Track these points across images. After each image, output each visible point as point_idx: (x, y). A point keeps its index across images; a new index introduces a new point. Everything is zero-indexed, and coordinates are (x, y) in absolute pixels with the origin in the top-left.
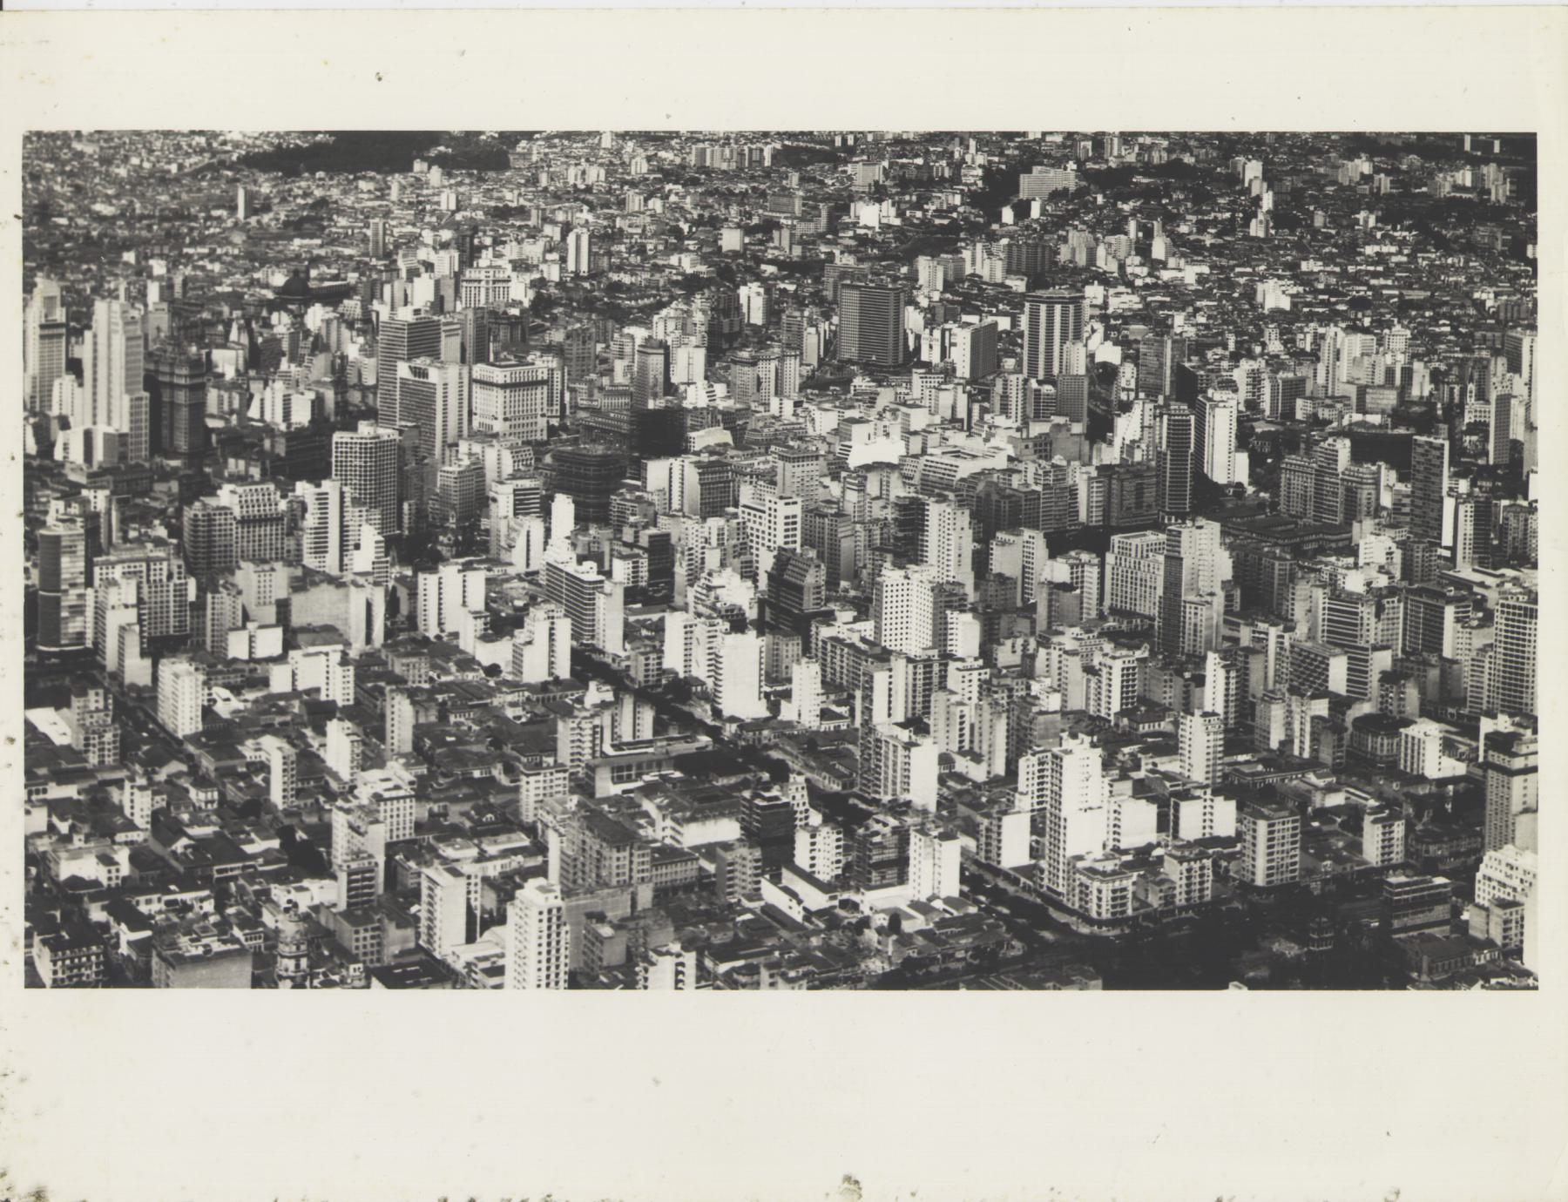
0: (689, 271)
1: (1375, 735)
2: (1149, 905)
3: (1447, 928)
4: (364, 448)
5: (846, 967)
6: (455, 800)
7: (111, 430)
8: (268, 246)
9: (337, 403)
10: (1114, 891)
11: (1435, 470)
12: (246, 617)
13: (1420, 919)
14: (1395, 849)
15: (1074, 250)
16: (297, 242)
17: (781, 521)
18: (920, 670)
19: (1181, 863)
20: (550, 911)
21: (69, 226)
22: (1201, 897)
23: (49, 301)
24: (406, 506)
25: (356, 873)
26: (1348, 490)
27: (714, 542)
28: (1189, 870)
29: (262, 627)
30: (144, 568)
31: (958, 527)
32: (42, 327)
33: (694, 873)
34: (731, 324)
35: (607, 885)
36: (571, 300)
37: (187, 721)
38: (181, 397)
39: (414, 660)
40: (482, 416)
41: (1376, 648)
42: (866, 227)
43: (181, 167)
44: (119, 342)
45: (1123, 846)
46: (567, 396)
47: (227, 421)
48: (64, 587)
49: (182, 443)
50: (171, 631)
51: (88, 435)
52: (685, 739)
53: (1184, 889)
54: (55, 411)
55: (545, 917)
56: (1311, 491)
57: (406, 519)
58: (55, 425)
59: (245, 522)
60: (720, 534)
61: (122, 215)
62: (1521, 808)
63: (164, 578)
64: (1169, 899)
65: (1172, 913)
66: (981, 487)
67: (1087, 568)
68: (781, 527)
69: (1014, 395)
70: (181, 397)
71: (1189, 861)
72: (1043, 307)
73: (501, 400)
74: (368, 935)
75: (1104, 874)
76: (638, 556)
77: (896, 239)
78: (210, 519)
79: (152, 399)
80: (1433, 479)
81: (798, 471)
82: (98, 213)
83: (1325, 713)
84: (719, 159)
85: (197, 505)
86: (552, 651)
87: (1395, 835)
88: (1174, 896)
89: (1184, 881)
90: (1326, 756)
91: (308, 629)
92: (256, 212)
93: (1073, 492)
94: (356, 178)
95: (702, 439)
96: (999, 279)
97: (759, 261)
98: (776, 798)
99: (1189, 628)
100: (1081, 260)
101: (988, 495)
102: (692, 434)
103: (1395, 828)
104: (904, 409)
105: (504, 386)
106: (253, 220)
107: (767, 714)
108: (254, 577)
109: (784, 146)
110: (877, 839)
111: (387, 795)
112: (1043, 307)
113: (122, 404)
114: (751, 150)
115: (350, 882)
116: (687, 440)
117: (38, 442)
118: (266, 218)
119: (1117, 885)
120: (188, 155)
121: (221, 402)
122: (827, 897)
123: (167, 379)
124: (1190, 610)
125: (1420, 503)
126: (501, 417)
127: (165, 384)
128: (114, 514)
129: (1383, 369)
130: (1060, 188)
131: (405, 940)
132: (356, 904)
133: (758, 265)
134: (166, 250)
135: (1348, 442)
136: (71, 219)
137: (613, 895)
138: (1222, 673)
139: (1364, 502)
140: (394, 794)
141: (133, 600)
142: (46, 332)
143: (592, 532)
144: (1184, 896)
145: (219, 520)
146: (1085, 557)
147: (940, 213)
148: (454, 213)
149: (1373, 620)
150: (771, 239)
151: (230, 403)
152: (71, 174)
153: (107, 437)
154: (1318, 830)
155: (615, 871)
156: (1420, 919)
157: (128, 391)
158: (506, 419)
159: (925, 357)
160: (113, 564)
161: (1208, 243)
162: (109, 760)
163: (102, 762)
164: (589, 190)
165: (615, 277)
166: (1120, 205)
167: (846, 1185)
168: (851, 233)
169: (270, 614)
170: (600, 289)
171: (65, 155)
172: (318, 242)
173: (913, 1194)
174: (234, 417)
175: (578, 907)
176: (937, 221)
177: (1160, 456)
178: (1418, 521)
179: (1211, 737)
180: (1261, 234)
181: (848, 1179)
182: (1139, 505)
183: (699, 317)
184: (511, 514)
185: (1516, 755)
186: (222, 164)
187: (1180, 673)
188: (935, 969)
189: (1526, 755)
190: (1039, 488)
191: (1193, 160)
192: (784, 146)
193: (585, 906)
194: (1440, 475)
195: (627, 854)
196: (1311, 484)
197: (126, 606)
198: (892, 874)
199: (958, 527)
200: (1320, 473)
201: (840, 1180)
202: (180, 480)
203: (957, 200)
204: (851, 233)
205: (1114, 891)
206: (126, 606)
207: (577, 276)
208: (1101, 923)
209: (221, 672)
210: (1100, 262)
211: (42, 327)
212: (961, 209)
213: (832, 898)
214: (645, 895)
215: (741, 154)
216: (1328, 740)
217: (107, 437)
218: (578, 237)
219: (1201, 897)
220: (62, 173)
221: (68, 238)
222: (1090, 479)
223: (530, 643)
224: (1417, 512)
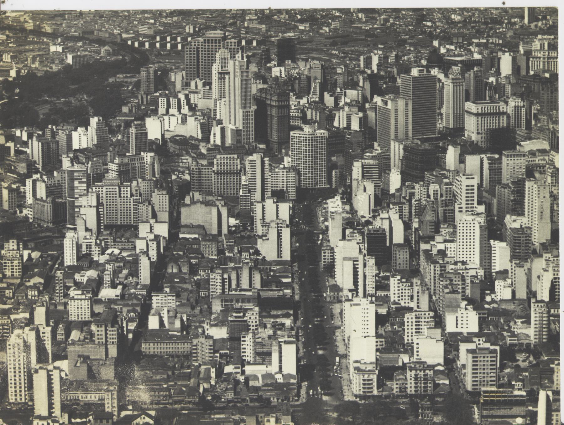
7: (234, 128)
10: (364, 380)
12: (154, 216)
13: (502, 412)
17: (464, 188)
22: (426, 391)
24: (334, 173)
28: (416, 375)
30: (117, 189)
31: (542, 197)
32: (219, 73)
35: (92, 342)
37: (69, 261)
48: (76, 196)
63: (129, 196)
70: (274, 112)
75: (364, 371)
81: (511, 162)
88: (406, 388)
91: (186, 226)
105: (477, 115)
106: (533, 25)
118: (540, 24)
126: (475, 132)
128: (156, 165)
134: (460, 40)
137: (94, 348)
141: (94, 203)
144: (413, 389)
156: (502, 412)
157: (242, 108)
158: (478, 133)
160: (102, 186)
162: (16, 274)
163: (12, 275)
184: (360, 178)
193: (79, 351)
195: (103, 329)
197: (91, 207)
202: (264, 157)
206: (91, 207)
213: (236, 368)
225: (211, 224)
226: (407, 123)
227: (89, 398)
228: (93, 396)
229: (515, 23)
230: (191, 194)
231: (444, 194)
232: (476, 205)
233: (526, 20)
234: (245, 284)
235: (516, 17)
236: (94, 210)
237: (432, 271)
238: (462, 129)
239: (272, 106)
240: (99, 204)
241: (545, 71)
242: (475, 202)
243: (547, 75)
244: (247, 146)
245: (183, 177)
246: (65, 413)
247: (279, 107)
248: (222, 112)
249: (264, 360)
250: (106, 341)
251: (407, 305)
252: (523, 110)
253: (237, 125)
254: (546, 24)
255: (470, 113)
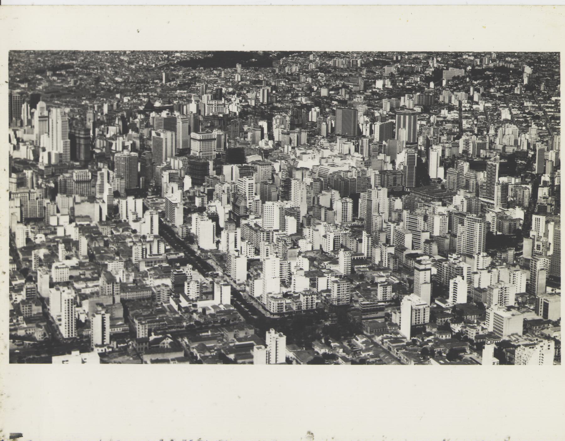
0: (304, 103)
1: (411, 260)
2: (292, 309)
3: (383, 319)
4: (125, 158)
5: (177, 323)
6: (88, 270)
7: (57, 152)
8: (168, 93)
9: (140, 145)
10: (278, 304)
11: (493, 174)
12: (58, 211)
14: (388, 295)
15: (444, 97)
16: (178, 91)
17: (247, 185)
18: (265, 234)
19: (304, 296)
20: (68, 300)
21: (105, 85)
22: (312, 307)
23: (42, 108)
24: (141, 179)
25: (29, 289)
26: (467, 180)
27: (226, 192)
28: (307, 299)
29: (62, 215)
31: (301, 189)
32: (39, 117)
33: (150, 294)
34: (298, 121)
36: (256, 112)
38: (82, 141)
39: (106, 227)
40: (194, 150)
41: (423, 231)
42: (378, 89)
43: (156, 65)
44: (60, 122)
45: (296, 291)
46: (227, 144)
47: (102, 150)
49: (82, 157)
50: (38, 216)
51: (49, 154)
52: (176, 254)
53: (305, 304)
54: (42, 146)
55: (67, 302)
56: (456, 181)
57: (141, 183)
58: (41, 150)
59: (78, 182)
60: (228, 189)
61: (124, 82)
62: (424, 282)
64: (299, 307)
65: (301, 312)
66: (335, 176)
67: (348, 204)
68: (247, 187)
69: (365, 146)
70: (82, 141)
71: (307, 295)
72: (402, 116)
73: (199, 145)
74: (27, 308)
75: (277, 298)
76: (204, 196)
77: (387, 93)
78: (65, 181)
79: (71, 142)
80: (493, 177)
81: (264, 169)
82: (116, 81)
83: (393, 252)
84: (340, 63)
85: (61, 176)
86: (152, 226)
87: (388, 291)
89: (305, 302)
90: (391, 267)
91: (78, 217)
92: (170, 81)
93: (369, 179)
94: (214, 70)
95: (372, 174)
96: (411, 107)
97: (332, 99)
98: (181, 272)
99: (374, 224)
100: (447, 101)
101: (337, 179)
102: (247, 157)
103: (388, 288)
104: (322, 150)
105: (200, 140)
106: (168, 84)
107: (216, 248)
108: (61, 199)
109: (374, 60)
110: (205, 285)
111: (59, 267)
112: (402, 116)
113: (61, 143)
114: (353, 61)
115: (27, 292)
116: (246, 159)
117: (34, 156)
118: (172, 83)
119: (279, 302)
120: (160, 61)
121: (100, 144)
122: (187, 303)
123: (77, 135)
124: (374, 218)
125: (489, 185)
127: (77, 137)
129: (513, 140)
130: (456, 75)
131: (38, 310)
132: (29, 299)
133: (331, 101)
134: (132, 94)
135: (468, 164)
136: (106, 83)
138: (366, 238)
139: (471, 185)
140: (62, 266)
141: (19, 205)
142: (41, 119)
143: (195, 188)
144: (305, 307)
145: (68, 181)
146: (348, 200)
147: (409, 84)
148: (239, 82)
149: (423, 222)
150: (339, 93)
151: (103, 144)
152: (115, 67)
153: (56, 154)
154: (369, 289)
155: (107, 291)
157: (63, 139)
159: (364, 134)
161: (497, 96)
164: (292, 74)
165: (275, 105)
166: (473, 82)
167: (308, 435)
168: (371, 91)
169: (66, 211)
170: (268, 109)
171: (117, 61)
172: (186, 91)
173: (333, 438)
174: (104, 149)
175: (93, 301)
176: (408, 87)
177: (405, 167)
178: (488, 191)
179: (346, 258)
180: (519, 93)
181: (309, 433)
182: (395, 184)
183: (288, 118)
185: (422, 264)
186: (171, 65)
187: (355, 238)
188: (210, 325)
189: (425, 265)
190: (356, 177)
191: (513, 66)
192: (374, 60)
194: (495, 175)
195: (111, 285)
196: (456, 178)
198: (210, 296)
199: (301, 189)
200: (458, 174)
201: (306, 432)
203: (419, 79)
204: (371, 91)
205: (278, 304)
207: (262, 104)
208: (274, 314)
209: (43, 229)
210: (453, 102)
211: (39, 117)
212: (419, 83)
213: (189, 303)
214: (118, 299)
215: (349, 62)
216: (392, 260)
217: (56, 154)
218: (263, 91)
219: (312, 307)
220: (112, 67)
221: (103, 89)
222: (375, 175)
223: (144, 222)
224: (488, 188)
225: (94, 214)
226: (172, 146)
227: (116, 330)
228: (119, 329)
229: (157, 83)
230: (73, 196)
231: (233, 189)
232: (254, 195)
233: (164, 82)
234: (155, 251)
235: (157, 79)
236: (19, 209)
237: (262, 237)
238: (189, 150)
239: (80, 138)
240: (21, 206)
241: (219, 113)
242: (254, 194)
243: (221, 115)
244: (68, 164)
245: (49, 185)
246: (114, 341)
247: (85, 138)
248: (45, 141)
249: (207, 297)
250: (113, 293)
251: (252, 258)
252: (223, 137)
253: (59, 150)
254: (176, 84)
255: (195, 140)
